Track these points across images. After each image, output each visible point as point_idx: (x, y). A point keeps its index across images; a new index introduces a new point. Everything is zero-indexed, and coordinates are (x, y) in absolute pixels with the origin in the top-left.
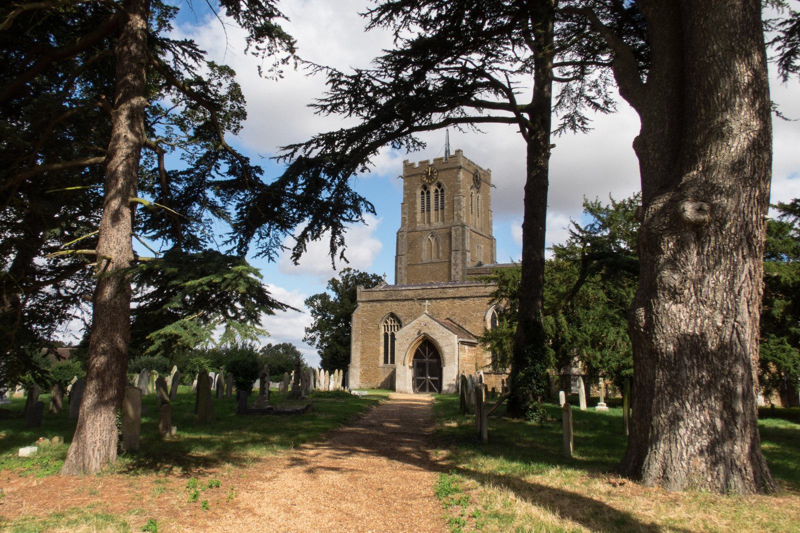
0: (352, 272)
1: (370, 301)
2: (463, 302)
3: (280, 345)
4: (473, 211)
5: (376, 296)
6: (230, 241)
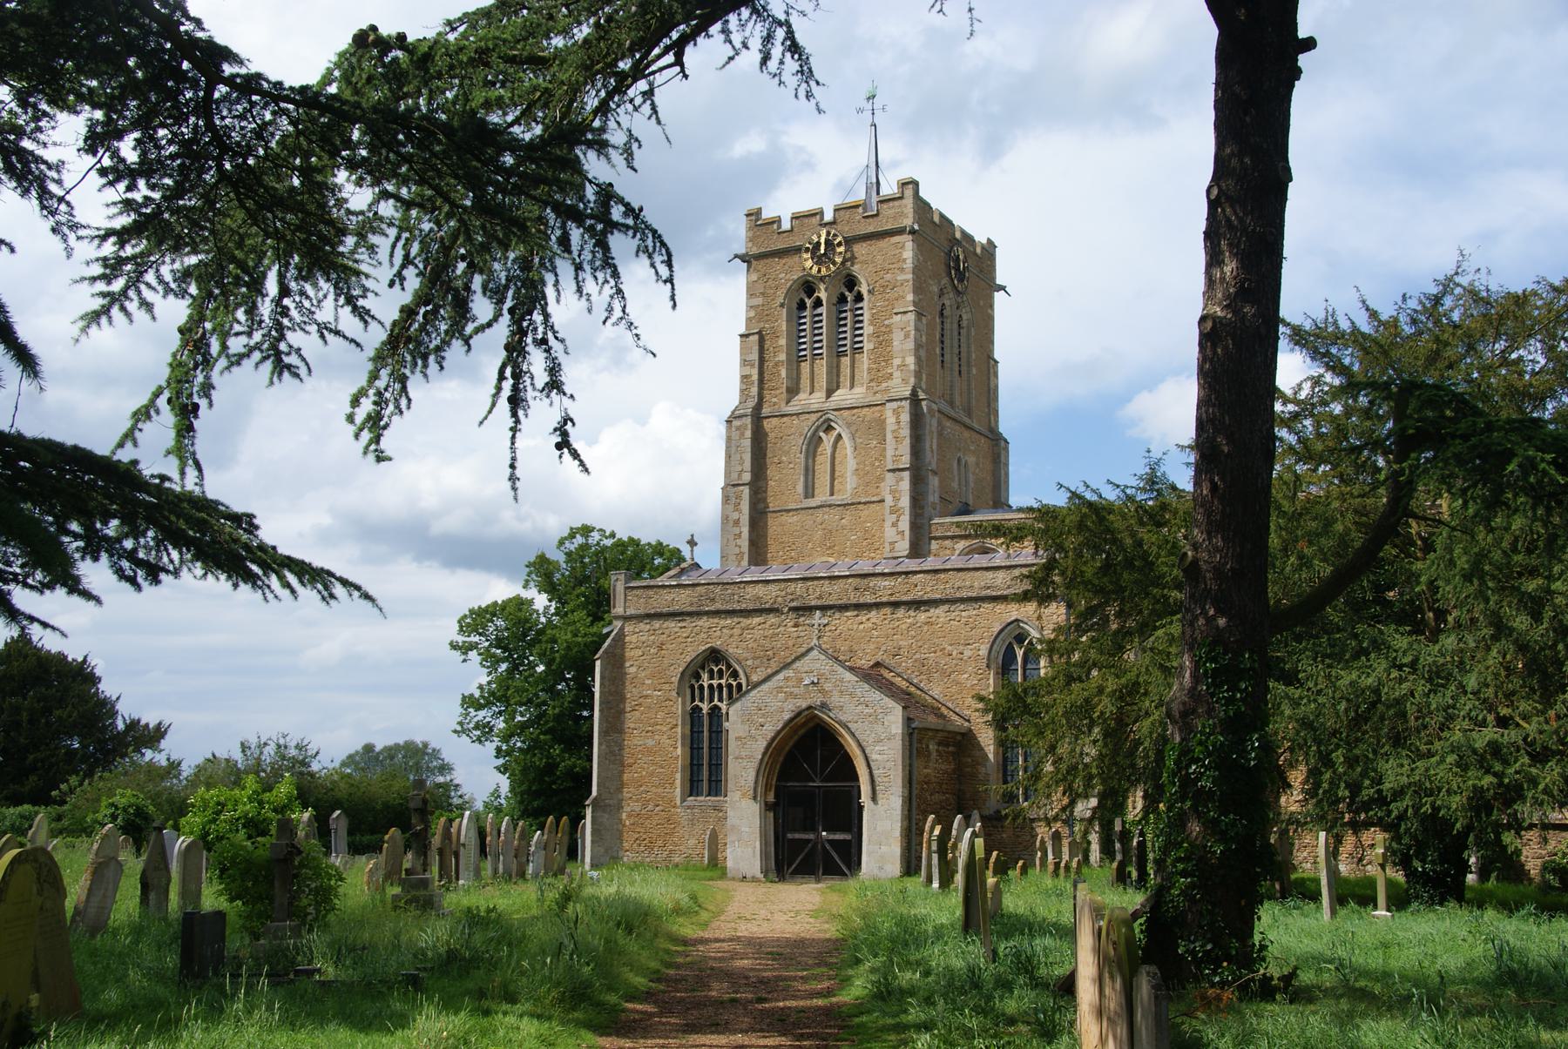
0: (596, 536)
1: (649, 616)
2: (922, 617)
3: (397, 745)
4: (947, 357)
5: (662, 601)
6: (106, 310)
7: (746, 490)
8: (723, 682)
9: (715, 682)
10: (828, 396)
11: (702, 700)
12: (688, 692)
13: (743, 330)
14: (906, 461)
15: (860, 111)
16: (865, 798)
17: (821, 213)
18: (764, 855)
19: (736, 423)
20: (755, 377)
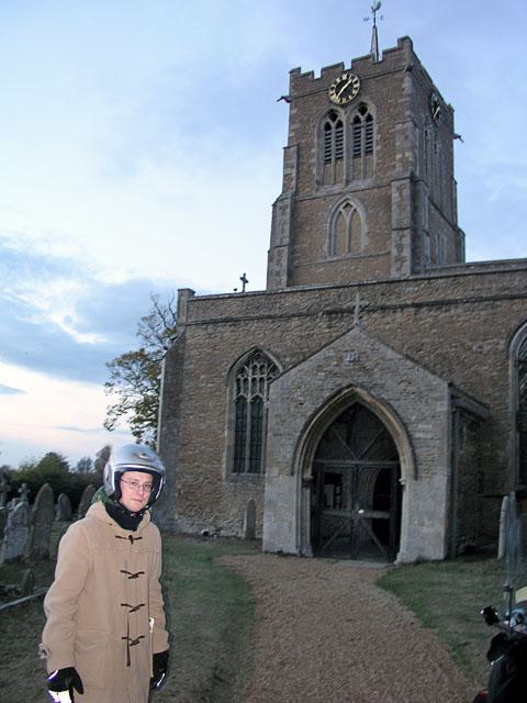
7: (286, 250)
8: (265, 376)
9: (258, 376)
10: (347, 184)
11: (246, 390)
12: (235, 384)
13: (286, 145)
14: (407, 221)
15: (366, 19)
16: (405, 478)
17: (342, 64)
18: (300, 530)
19: (280, 204)
20: (294, 175)
